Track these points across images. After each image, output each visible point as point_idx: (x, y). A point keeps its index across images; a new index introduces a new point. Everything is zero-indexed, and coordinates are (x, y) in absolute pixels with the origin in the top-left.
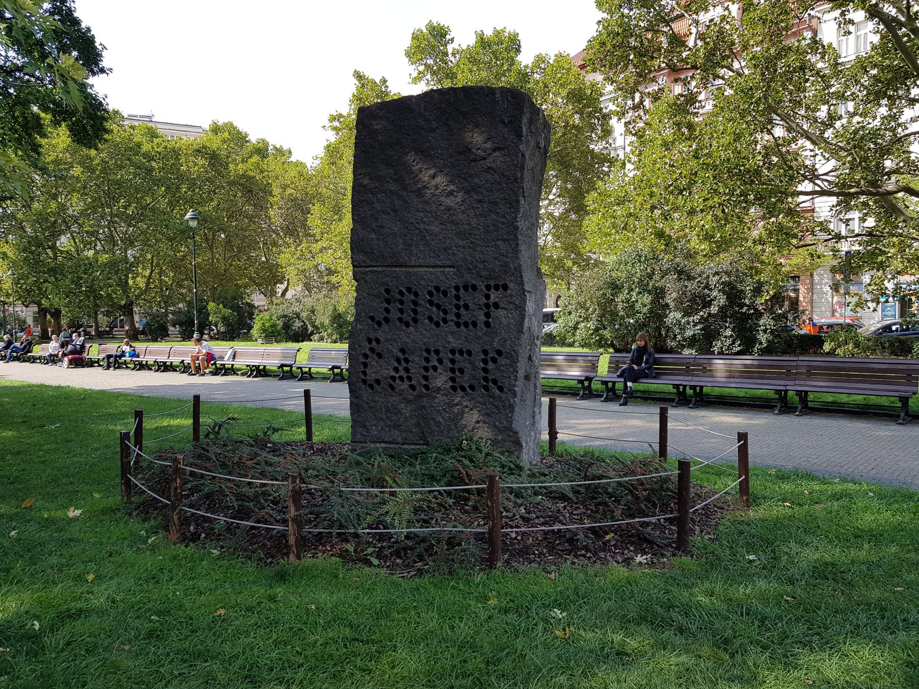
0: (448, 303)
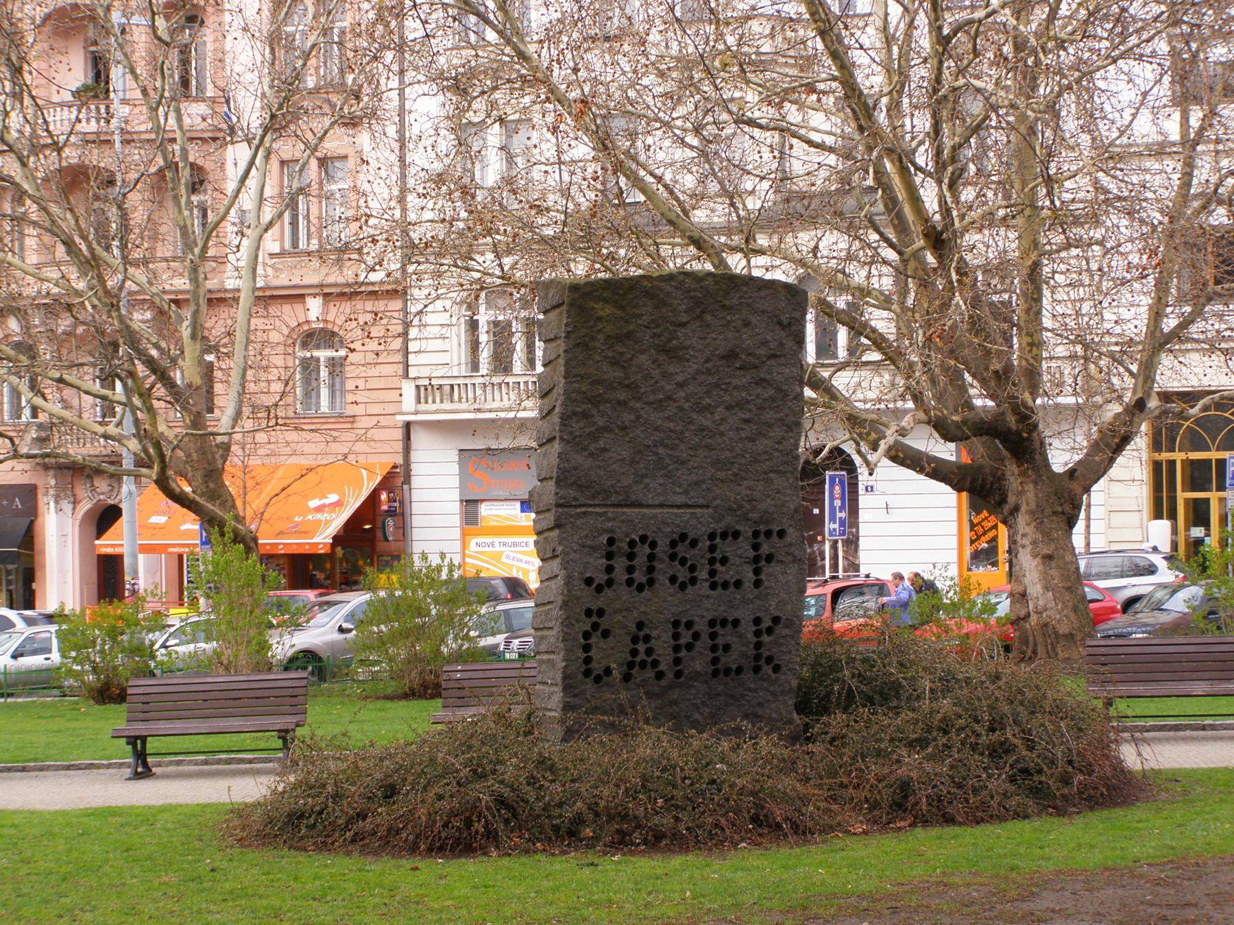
0: (697, 556)
